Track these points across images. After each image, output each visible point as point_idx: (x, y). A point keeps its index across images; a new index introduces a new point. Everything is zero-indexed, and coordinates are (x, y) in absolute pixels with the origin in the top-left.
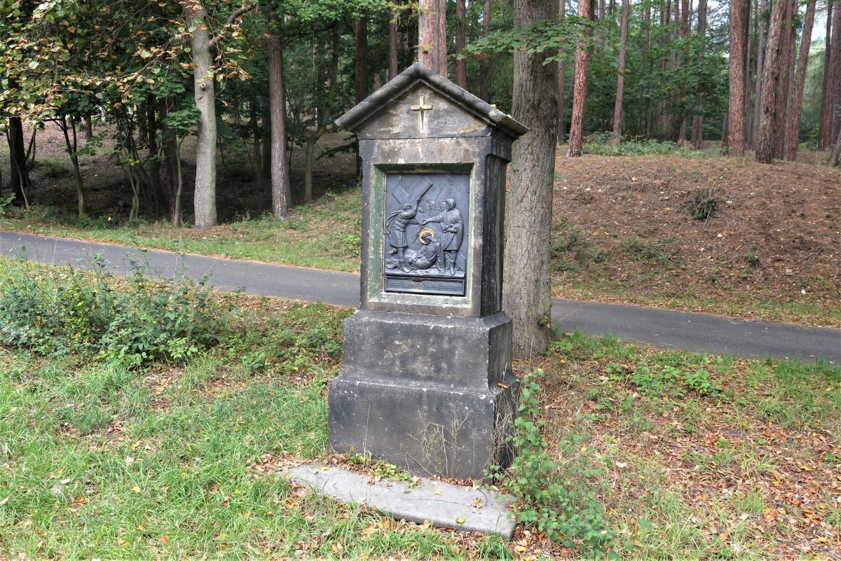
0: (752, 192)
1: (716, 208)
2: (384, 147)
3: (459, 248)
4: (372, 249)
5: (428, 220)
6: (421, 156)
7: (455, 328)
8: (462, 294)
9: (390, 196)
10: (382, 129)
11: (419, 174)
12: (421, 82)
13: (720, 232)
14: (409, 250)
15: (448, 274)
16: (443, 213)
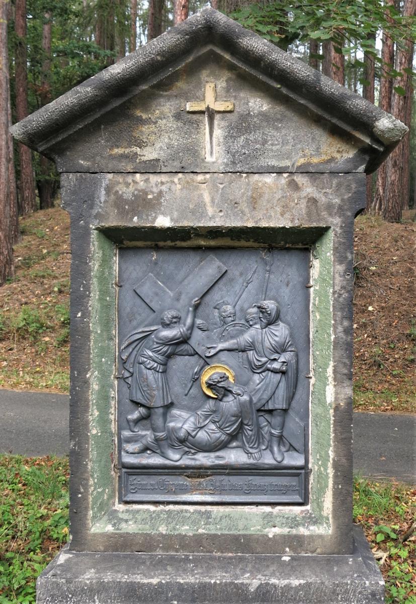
0: (394, 256)
1: (360, 276)
2: (121, 189)
3: (289, 404)
4: (96, 413)
5: (221, 346)
6: (210, 211)
7: (308, 585)
8: (299, 499)
9: (129, 295)
10: (117, 151)
11: (198, 248)
12: (212, 52)
13: (371, 304)
14: (175, 412)
15: (268, 460)
16: (252, 331)
